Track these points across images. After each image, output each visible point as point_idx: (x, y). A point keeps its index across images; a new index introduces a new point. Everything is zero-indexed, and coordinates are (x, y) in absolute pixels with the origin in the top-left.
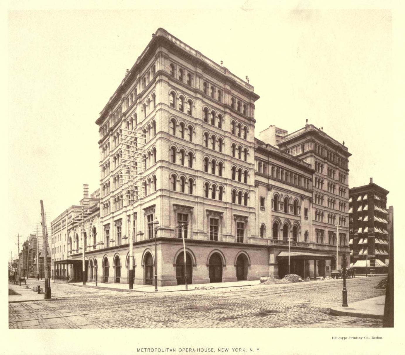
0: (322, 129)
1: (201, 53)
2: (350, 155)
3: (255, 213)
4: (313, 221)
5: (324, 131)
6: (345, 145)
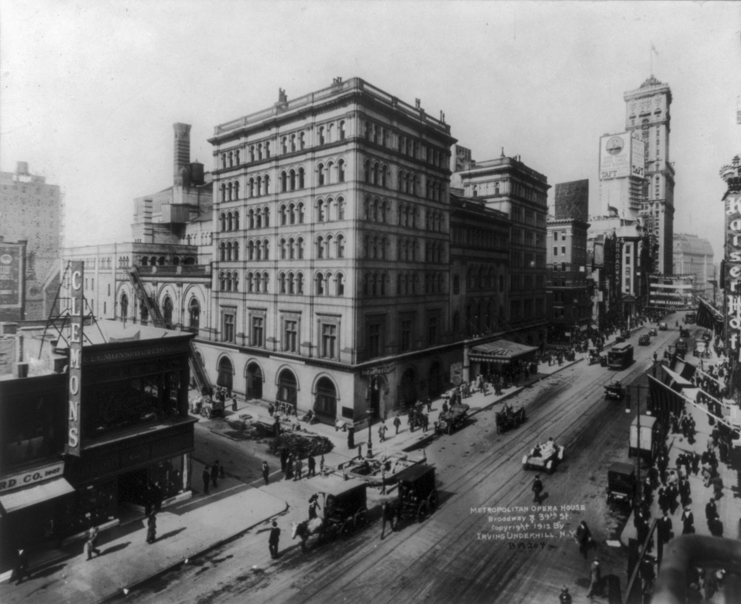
5: (522, 160)
6: (448, 121)
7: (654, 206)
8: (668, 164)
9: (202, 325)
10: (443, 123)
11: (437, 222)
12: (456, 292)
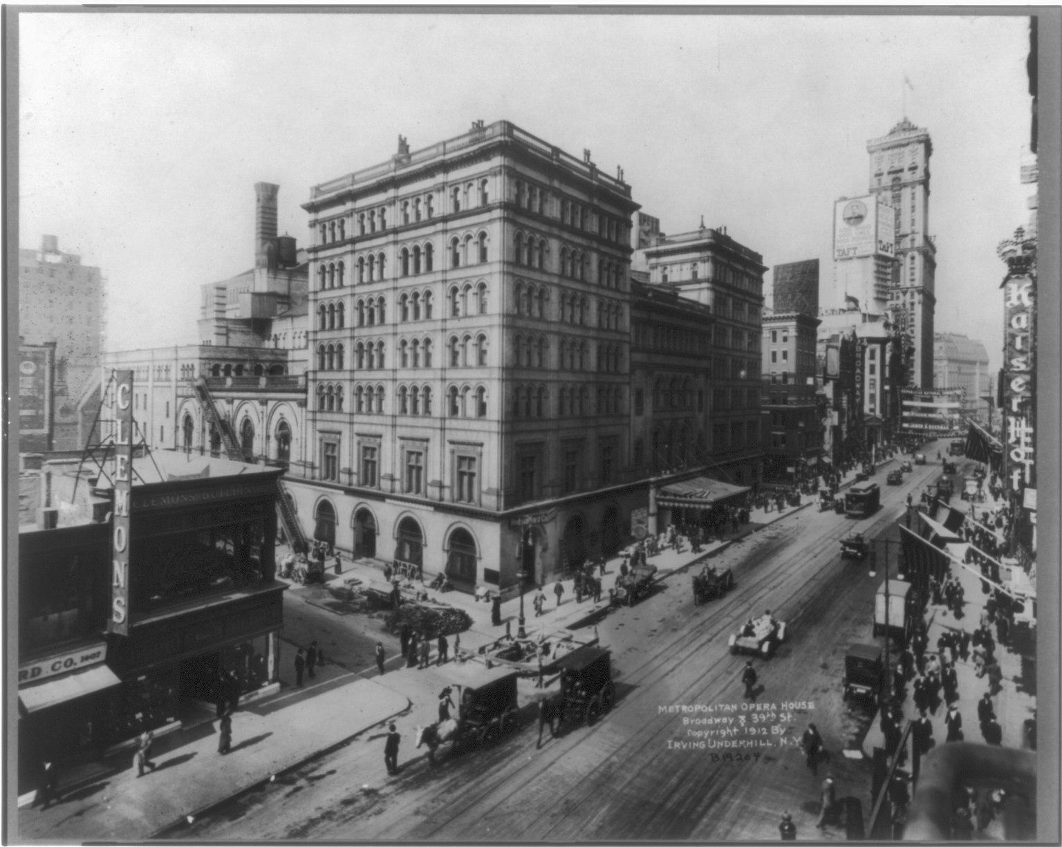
5: (729, 233)
6: (627, 180)
7: (908, 295)
8: (926, 238)
9: (294, 457)
10: (622, 183)
11: (613, 317)
12: (639, 412)
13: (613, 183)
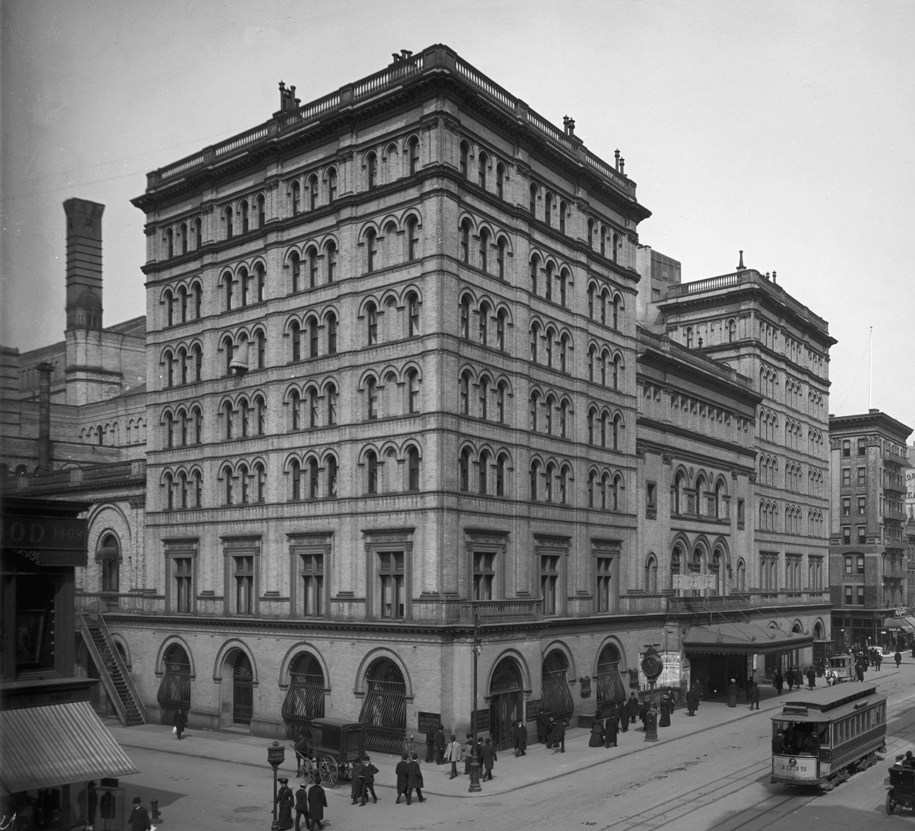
0: (774, 276)
1: (455, 54)
2: (833, 341)
3: (635, 528)
4: (756, 531)
6: (629, 171)
10: (623, 177)
12: (651, 512)
13: (611, 175)
